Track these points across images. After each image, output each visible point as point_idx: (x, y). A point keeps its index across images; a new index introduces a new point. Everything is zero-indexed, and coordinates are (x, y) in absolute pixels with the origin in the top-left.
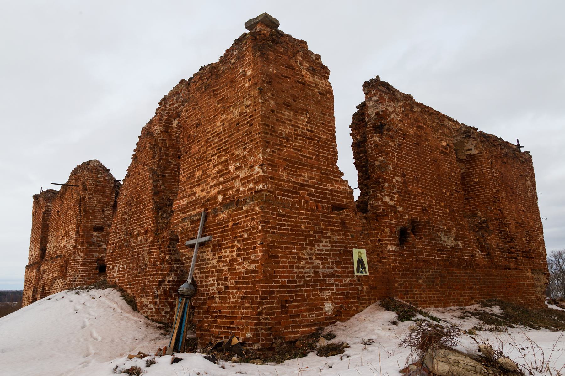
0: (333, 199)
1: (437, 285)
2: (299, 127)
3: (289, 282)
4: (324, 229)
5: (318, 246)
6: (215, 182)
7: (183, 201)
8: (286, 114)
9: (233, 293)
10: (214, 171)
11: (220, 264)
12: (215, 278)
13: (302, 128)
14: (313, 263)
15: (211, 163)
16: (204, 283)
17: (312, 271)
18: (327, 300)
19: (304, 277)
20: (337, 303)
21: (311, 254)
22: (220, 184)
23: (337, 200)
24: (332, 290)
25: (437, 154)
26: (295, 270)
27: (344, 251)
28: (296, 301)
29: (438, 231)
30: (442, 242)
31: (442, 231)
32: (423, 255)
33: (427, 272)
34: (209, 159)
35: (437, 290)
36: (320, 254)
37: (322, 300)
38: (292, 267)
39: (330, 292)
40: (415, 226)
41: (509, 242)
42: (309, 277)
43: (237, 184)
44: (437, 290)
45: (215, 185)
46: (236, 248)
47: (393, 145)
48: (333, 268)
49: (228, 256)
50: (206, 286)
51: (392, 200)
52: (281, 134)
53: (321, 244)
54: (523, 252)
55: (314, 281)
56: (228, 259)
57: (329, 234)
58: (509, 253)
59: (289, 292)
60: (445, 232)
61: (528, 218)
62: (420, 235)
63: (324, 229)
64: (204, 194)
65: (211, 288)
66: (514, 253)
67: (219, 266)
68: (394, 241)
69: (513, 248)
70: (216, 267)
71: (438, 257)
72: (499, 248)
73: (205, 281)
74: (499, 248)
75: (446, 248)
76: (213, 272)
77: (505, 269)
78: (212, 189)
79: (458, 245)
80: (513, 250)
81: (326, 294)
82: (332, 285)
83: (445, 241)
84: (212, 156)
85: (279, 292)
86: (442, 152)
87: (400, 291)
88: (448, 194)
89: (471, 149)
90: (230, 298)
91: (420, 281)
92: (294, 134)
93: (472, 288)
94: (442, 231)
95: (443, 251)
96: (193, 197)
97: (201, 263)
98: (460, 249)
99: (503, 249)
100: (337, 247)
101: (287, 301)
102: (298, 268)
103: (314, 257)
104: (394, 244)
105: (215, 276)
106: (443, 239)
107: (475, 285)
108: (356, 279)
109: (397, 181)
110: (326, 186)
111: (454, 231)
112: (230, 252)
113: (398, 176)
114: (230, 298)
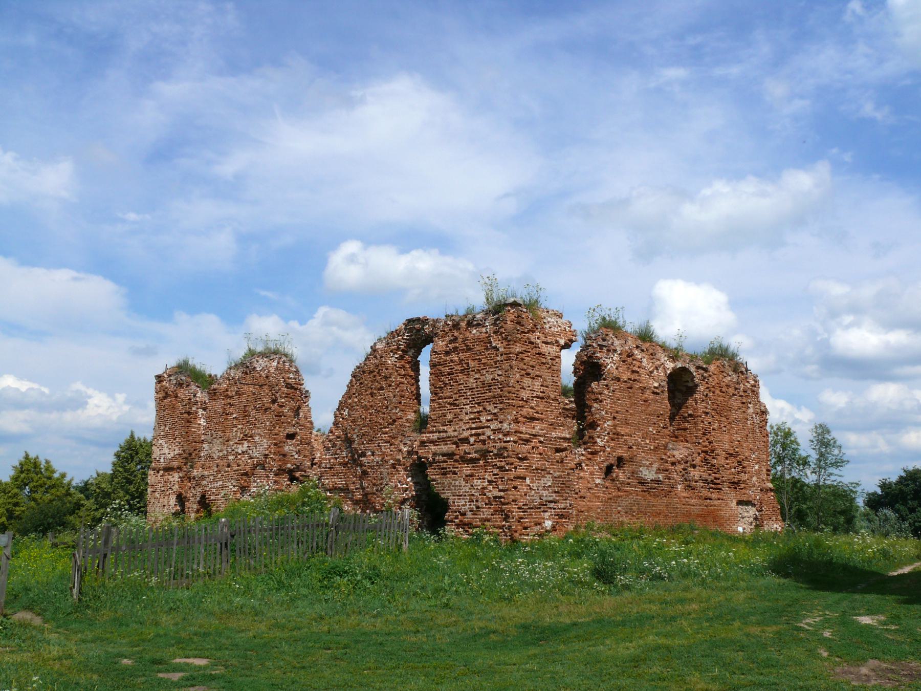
0: (555, 445)
1: (634, 512)
2: (534, 391)
3: (523, 505)
4: (548, 468)
5: (544, 480)
6: (468, 427)
7: (433, 436)
8: (527, 381)
9: (483, 512)
10: (467, 418)
11: (471, 490)
12: (467, 501)
13: (537, 391)
14: (539, 493)
15: (464, 411)
16: (456, 504)
17: (538, 498)
18: (547, 519)
19: (533, 502)
20: (554, 522)
21: (539, 486)
22: (472, 429)
23: (559, 445)
24: (551, 512)
25: (648, 395)
26: (528, 498)
27: (561, 484)
28: (526, 518)
29: (640, 466)
30: (643, 476)
31: (644, 465)
32: (625, 487)
33: (626, 501)
34: (462, 407)
35: (633, 516)
36: (544, 486)
37: (544, 519)
38: (525, 495)
39: (550, 513)
40: (620, 461)
41: (715, 473)
42: (536, 502)
43: (488, 432)
44: (633, 516)
45: (468, 429)
46: (486, 480)
47: (607, 393)
48: (552, 496)
49: (479, 485)
50: (459, 506)
51: (602, 441)
52: (523, 398)
53: (545, 479)
54: (729, 483)
55: (539, 505)
56: (479, 488)
57: (551, 472)
58: (713, 484)
59: (523, 512)
60: (647, 466)
61: (743, 449)
62: (624, 470)
63: (548, 468)
64: (456, 434)
65: (463, 507)
66: (719, 484)
67: (471, 492)
68: (600, 475)
69: (719, 479)
70: (468, 492)
71: (638, 488)
72: (702, 480)
73: (457, 502)
74: (702, 480)
75: (646, 480)
76: (465, 496)
77: (706, 499)
78: (464, 432)
79: (659, 478)
80: (718, 481)
81: (547, 515)
82: (551, 508)
83: (646, 475)
84: (464, 405)
85: (517, 512)
86: (654, 393)
87: (602, 515)
88: (654, 432)
89: (688, 382)
90: (480, 515)
91: (619, 508)
92: (532, 397)
93: (668, 515)
94: (644, 465)
95: (644, 483)
96: (445, 434)
97: (453, 488)
98: (660, 481)
99: (707, 480)
100: (556, 481)
101: (522, 518)
102: (529, 496)
103: (541, 488)
104: (600, 478)
105: (467, 499)
106: (644, 473)
107: (671, 513)
108: (568, 505)
109: (608, 425)
110: (551, 434)
111: (655, 466)
112: (481, 482)
113: (608, 420)
114: (480, 515)
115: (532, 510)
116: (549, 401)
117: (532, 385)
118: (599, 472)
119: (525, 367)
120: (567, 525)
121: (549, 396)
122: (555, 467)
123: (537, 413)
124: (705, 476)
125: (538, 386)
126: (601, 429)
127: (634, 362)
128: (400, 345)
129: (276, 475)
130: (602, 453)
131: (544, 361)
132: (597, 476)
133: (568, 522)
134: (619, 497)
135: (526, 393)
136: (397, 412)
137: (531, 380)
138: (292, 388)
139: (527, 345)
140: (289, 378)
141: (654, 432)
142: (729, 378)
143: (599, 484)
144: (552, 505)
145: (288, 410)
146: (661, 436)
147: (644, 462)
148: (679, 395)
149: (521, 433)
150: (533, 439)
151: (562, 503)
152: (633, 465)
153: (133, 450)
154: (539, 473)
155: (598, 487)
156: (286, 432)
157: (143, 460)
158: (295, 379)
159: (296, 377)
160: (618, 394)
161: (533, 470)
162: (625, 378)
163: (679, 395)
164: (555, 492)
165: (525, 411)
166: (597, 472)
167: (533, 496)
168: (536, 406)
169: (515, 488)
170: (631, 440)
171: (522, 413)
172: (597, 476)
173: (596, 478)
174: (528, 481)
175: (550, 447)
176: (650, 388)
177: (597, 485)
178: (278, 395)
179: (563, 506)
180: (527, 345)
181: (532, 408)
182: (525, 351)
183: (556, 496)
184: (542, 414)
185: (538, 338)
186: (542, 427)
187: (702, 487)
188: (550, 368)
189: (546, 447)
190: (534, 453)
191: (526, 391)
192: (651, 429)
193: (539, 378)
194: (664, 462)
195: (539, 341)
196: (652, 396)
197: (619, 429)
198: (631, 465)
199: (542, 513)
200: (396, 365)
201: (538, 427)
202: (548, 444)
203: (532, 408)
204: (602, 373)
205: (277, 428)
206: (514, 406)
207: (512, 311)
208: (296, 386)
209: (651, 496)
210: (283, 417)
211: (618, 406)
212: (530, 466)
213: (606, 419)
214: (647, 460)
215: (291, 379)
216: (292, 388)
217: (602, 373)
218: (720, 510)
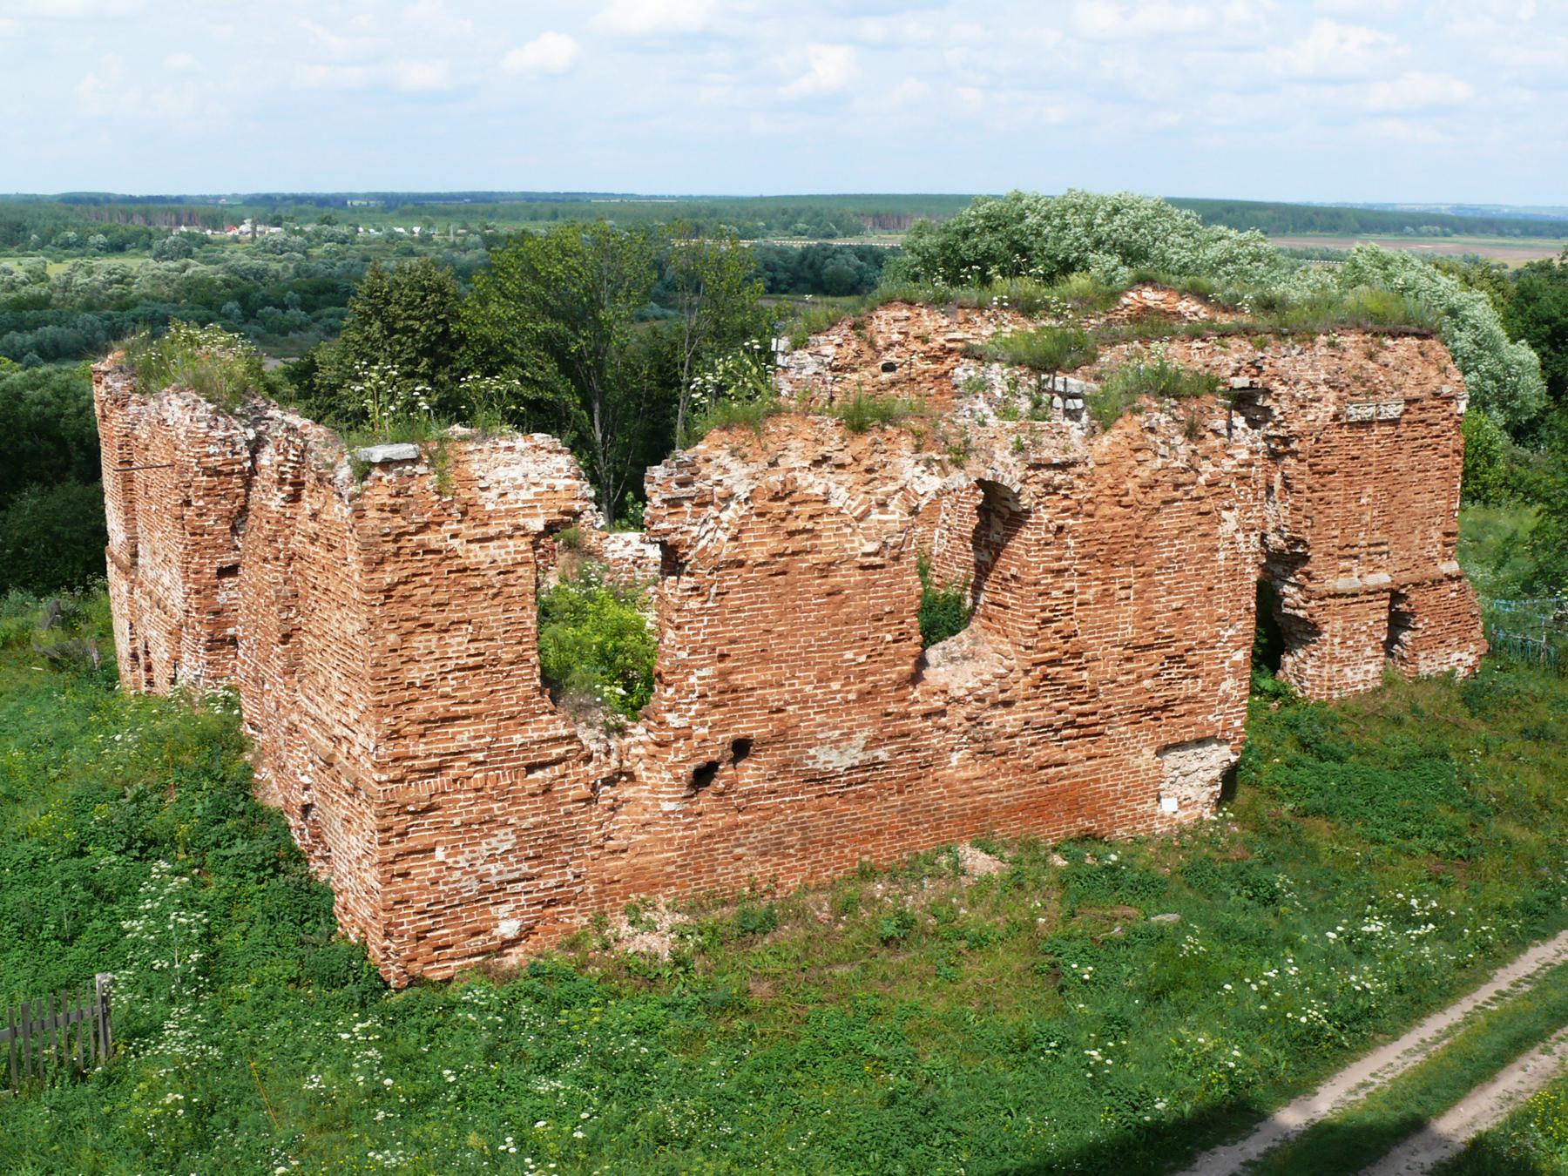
5: (488, 844)
19: (459, 893)
25: (847, 577)
26: (441, 888)
28: (443, 928)
32: (760, 799)
55: (480, 894)
57: (511, 821)
59: (430, 917)
66: (1096, 724)
81: (504, 910)
88: (863, 659)
106: (822, 758)
115: (459, 909)
116: (499, 668)
117: (438, 647)
118: (672, 786)
119: (415, 612)
120: (570, 918)
121: (498, 660)
122: (524, 808)
123: (461, 703)
124: (1041, 717)
125: (460, 644)
126: (677, 691)
127: (797, 508)
128: (283, 473)
129: (209, 649)
130: (681, 743)
131: (478, 582)
132: (666, 796)
133: (573, 911)
134: (737, 826)
135: (421, 670)
136: (291, 615)
137: (435, 637)
138: (218, 473)
139: (421, 561)
140: (208, 455)
141: (863, 659)
142: (1159, 462)
143: (673, 812)
144: (519, 886)
145: (216, 521)
146: (884, 662)
147: (821, 736)
148: (997, 525)
149: (415, 757)
150: (451, 761)
151: (554, 876)
152: (788, 748)
153: (376, 297)
154: (476, 831)
155: (669, 819)
156: (217, 565)
157: (399, 315)
158: (224, 454)
159: (223, 450)
160: (733, 601)
161: (456, 827)
162: (758, 554)
163: (997, 525)
164: (528, 859)
165: (419, 710)
166: (668, 786)
167: (459, 881)
168: (455, 690)
169: (405, 875)
170: (772, 695)
171: (412, 715)
172: (666, 796)
173: (664, 800)
174: (440, 854)
175: (509, 768)
176: (851, 559)
177: (666, 815)
178: (191, 491)
179: (552, 882)
180: (421, 561)
181: (445, 696)
182: (415, 575)
183: (531, 867)
184: (477, 702)
185: (454, 536)
186: (479, 730)
187: (1033, 744)
188: (495, 596)
189: (498, 768)
190: (457, 791)
191: (422, 665)
192: (849, 655)
193: (464, 626)
194: (895, 720)
195: (455, 543)
196: (857, 577)
197: (736, 679)
198: (778, 749)
199: (491, 908)
200: (284, 515)
201: (463, 734)
202: (503, 761)
203: (445, 696)
204: (683, 560)
205: (197, 559)
206: (387, 706)
207: (385, 480)
208: (226, 469)
209: (848, 802)
210: (206, 536)
211: (738, 625)
212: (446, 822)
213: (693, 667)
214: (835, 728)
215: (213, 455)
216: (218, 473)
217: (683, 560)
218: (1096, 781)
